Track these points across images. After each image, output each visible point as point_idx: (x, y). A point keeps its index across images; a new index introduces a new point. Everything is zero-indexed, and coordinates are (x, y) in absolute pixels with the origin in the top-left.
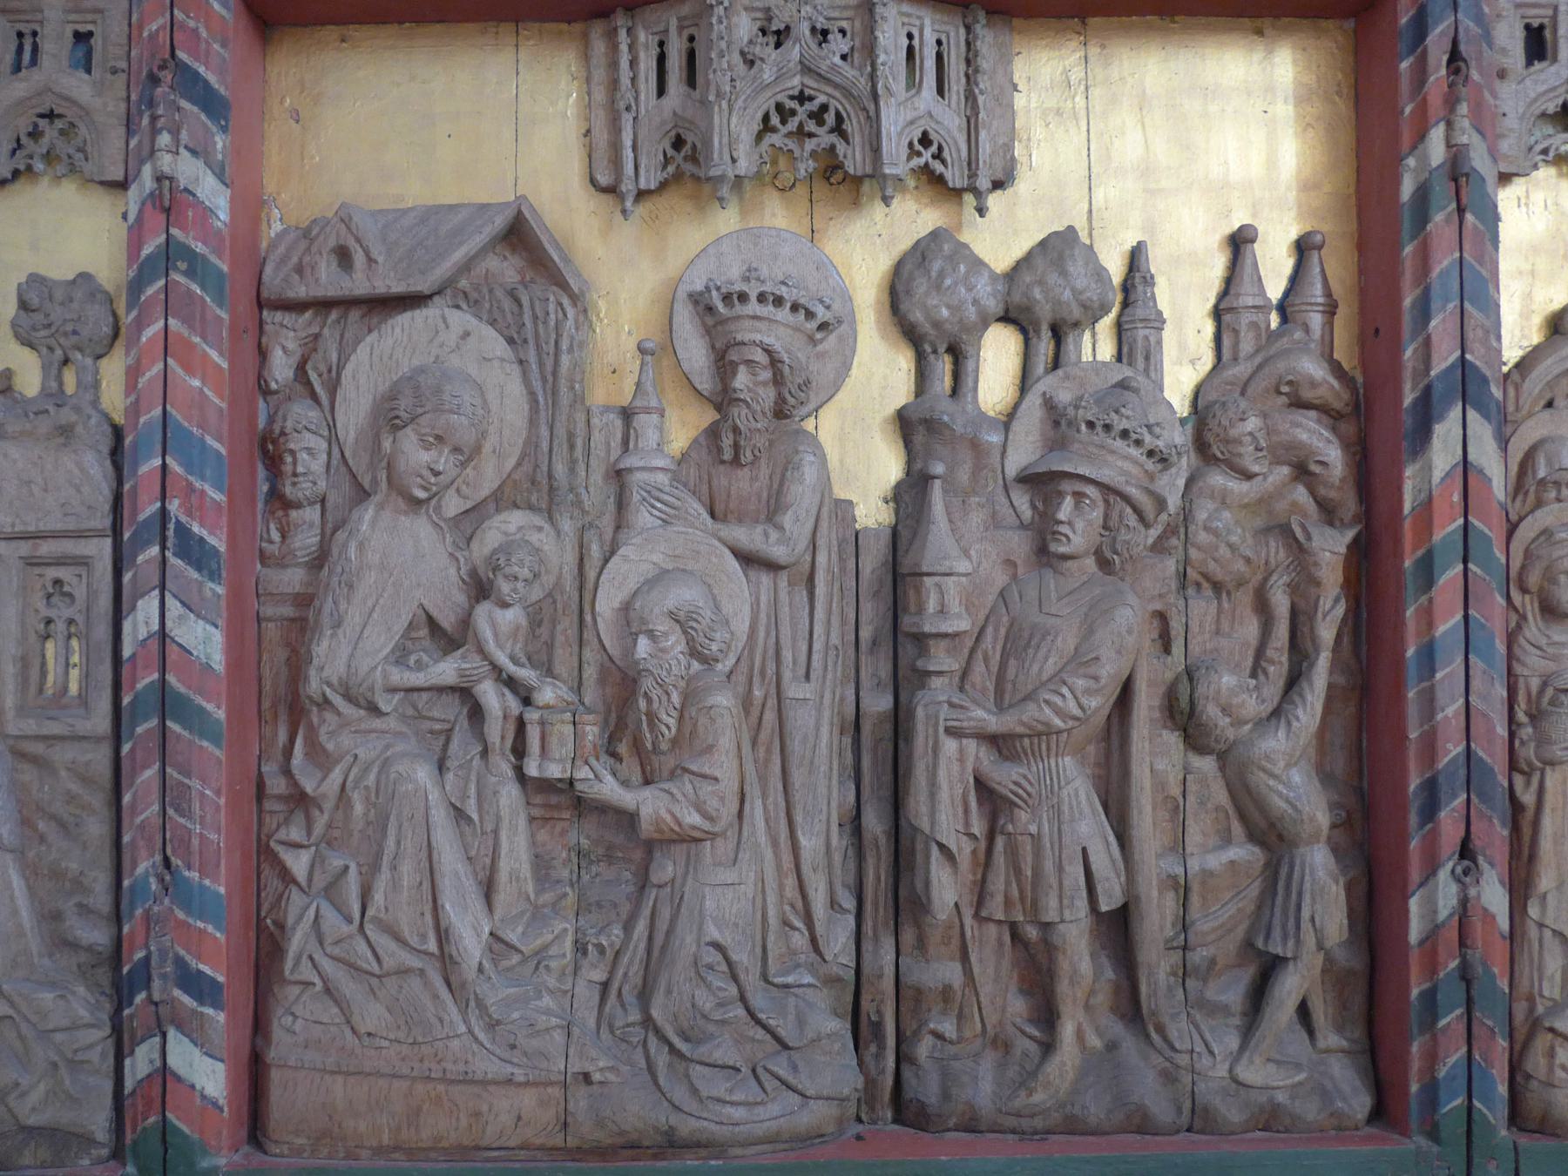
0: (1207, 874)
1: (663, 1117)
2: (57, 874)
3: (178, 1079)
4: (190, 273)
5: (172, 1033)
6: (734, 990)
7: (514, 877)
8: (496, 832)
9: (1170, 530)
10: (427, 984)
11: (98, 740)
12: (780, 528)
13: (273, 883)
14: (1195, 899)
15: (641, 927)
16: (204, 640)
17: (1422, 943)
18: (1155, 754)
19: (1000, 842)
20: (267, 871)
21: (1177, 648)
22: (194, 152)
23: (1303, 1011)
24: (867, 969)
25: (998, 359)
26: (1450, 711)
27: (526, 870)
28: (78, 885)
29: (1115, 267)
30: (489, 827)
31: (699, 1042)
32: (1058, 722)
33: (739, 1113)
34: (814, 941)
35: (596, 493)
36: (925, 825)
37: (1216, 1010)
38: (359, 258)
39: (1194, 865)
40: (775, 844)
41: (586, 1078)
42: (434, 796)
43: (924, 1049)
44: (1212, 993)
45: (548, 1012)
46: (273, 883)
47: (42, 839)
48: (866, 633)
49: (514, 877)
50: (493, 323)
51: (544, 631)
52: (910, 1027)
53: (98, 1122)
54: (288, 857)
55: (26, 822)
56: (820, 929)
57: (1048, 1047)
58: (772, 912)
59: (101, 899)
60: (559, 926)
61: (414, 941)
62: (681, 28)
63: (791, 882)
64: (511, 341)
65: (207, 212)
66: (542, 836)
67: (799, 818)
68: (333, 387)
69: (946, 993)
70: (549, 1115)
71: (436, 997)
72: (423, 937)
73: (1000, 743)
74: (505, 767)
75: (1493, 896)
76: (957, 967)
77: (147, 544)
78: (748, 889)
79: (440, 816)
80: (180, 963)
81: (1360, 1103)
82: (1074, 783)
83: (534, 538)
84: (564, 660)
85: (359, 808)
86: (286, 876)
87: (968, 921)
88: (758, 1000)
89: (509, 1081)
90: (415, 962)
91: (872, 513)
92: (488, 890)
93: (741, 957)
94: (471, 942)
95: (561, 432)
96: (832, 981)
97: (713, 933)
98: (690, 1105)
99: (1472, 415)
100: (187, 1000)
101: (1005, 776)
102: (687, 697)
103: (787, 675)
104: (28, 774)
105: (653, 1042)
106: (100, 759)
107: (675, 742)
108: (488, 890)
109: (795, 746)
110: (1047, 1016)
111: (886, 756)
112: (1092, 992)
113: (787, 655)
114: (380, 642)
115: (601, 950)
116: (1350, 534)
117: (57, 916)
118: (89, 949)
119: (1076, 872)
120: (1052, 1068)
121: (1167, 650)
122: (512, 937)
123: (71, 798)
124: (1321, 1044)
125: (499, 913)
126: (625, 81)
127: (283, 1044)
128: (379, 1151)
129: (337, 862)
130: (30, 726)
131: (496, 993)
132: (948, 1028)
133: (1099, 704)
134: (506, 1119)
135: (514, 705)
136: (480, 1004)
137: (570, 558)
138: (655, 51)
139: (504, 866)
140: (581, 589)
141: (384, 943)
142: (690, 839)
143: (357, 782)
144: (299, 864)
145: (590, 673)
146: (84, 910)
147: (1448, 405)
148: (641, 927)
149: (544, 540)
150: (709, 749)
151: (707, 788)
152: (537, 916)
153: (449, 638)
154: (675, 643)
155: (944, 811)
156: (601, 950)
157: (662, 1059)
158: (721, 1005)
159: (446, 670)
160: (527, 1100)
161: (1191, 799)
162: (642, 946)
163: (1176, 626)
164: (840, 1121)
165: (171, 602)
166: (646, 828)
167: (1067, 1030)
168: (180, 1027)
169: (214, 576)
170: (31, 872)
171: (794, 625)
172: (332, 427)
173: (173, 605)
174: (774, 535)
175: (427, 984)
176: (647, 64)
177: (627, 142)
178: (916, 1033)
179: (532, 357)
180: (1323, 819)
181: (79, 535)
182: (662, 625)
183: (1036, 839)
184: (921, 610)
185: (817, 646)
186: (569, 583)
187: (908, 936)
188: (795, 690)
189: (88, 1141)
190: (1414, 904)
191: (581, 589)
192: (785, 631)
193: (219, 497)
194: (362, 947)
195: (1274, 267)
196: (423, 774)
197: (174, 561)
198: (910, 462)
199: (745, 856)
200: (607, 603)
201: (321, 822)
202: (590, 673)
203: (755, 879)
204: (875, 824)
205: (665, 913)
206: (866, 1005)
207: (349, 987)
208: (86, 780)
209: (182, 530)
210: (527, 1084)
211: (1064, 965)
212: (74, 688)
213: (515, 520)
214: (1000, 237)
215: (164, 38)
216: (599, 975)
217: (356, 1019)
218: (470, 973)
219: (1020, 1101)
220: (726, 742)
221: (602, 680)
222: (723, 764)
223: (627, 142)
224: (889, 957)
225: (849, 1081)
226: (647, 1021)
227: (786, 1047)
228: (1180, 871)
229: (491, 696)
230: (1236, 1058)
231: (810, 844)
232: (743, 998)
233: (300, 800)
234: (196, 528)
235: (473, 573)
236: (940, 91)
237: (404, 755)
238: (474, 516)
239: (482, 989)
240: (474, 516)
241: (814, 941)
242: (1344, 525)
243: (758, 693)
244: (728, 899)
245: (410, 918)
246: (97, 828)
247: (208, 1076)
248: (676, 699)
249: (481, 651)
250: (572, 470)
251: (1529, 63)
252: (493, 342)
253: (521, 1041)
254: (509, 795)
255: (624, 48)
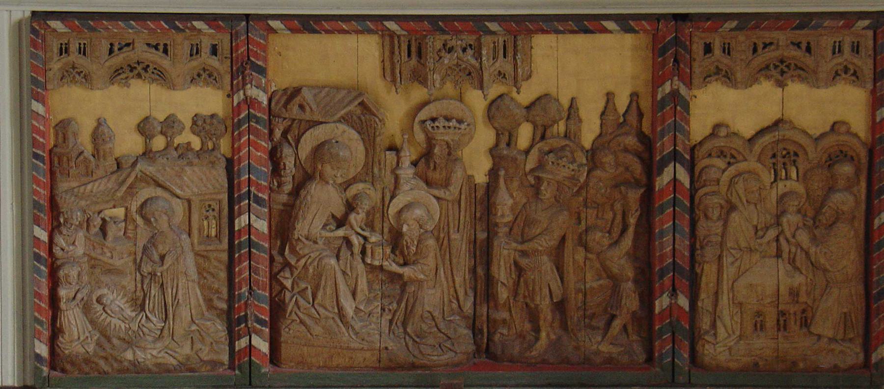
0: (592, 288)
1: (411, 359)
2: (210, 288)
3: (255, 348)
4: (257, 122)
5: (253, 336)
6: (434, 323)
7: (362, 291)
8: (357, 278)
9: (581, 188)
10: (335, 321)
11: (224, 251)
12: (449, 190)
13: (278, 288)
14: (588, 296)
15: (403, 305)
16: (262, 226)
17: (659, 313)
18: (575, 256)
19: (522, 279)
20: (274, 283)
21: (583, 223)
22: (257, 87)
23: (625, 327)
24: (478, 314)
25: (525, 134)
26: (668, 249)
27: (366, 288)
28: (218, 291)
29: (566, 103)
30: (354, 276)
31: (423, 338)
32: (540, 248)
33: (435, 358)
34: (459, 306)
35: (389, 179)
36: (497, 276)
37: (594, 328)
38: (308, 108)
39: (588, 286)
40: (447, 278)
41: (386, 348)
42: (337, 268)
43: (497, 337)
44: (594, 323)
45: (374, 329)
46: (277, 288)
47: (205, 278)
48: (478, 215)
49: (362, 291)
50: (353, 127)
51: (371, 217)
52: (492, 330)
53: (225, 358)
54: (285, 282)
55: (199, 273)
56: (462, 303)
57: (537, 339)
58: (446, 300)
59: (225, 295)
60: (376, 304)
61: (330, 309)
62: (416, 40)
63: (452, 290)
64: (359, 133)
65: (260, 103)
66: (370, 276)
67: (455, 273)
68: (298, 142)
69: (504, 321)
70: (375, 358)
71: (338, 325)
72: (333, 308)
73: (524, 254)
74: (358, 258)
75: (683, 302)
76: (508, 313)
77: (244, 200)
78: (439, 294)
79: (339, 275)
80: (256, 316)
81: (642, 357)
82: (547, 264)
83: (368, 192)
84: (378, 226)
85: (311, 271)
86: (284, 287)
87: (511, 301)
88: (442, 326)
89: (362, 349)
90: (331, 315)
91: (481, 178)
92: (354, 294)
93: (436, 314)
94: (349, 310)
95: (376, 160)
96: (465, 317)
97: (428, 309)
98: (419, 356)
99: (677, 165)
100: (258, 326)
101: (524, 262)
102: (419, 242)
103: (452, 231)
104: (201, 261)
105: (407, 337)
106: (225, 256)
107: (415, 254)
108: (354, 294)
109: (454, 251)
110: (537, 330)
111: (483, 253)
112: (553, 322)
113: (452, 225)
114: (318, 223)
115: (390, 310)
116: (642, 190)
117: (211, 300)
118: (221, 310)
119: (546, 291)
120: (538, 345)
121: (580, 223)
122: (362, 308)
123: (216, 267)
124: (631, 339)
125: (357, 300)
126: (397, 53)
127: (285, 335)
128: (319, 367)
129: (303, 286)
130: (203, 247)
131: (358, 325)
132: (505, 332)
133: (554, 243)
134: (361, 359)
135: (362, 241)
136: (353, 329)
137: (380, 196)
138: (407, 44)
139: (359, 288)
140: (383, 205)
141: (322, 311)
142: (420, 282)
143: (310, 264)
144: (288, 283)
145: (386, 230)
146: (219, 298)
147: (670, 163)
148: (403, 305)
149: (371, 192)
150: (427, 257)
151: (425, 268)
152: (369, 301)
153: (341, 222)
154: (415, 226)
155: (502, 273)
156: (390, 310)
157: (410, 343)
158: (430, 328)
159: (341, 232)
160: (368, 355)
161: (588, 266)
162: (403, 312)
163: (583, 215)
164: (467, 359)
165: (252, 215)
166: (406, 278)
167: (543, 334)
168: (256, 333)
169: (264, 206)
170: (202, 287)
171: (454, 216)
172: (297, 154)
173: (253, 217)
174: (447, 193)
175: (335, 321)
176: (404, 47)
177: (398, 71)
178: (494, 333)
179: (367, 139)
180: (630, 274)
181: (219, 193)
182: (411, 222)
183: (534, 280)
184: (496, 215)
185: (461, 222)
186: (379, 205)
187: (492, 304)
188: (454, 236)
189: (222, 364)
190: (657, 303)
191: (383, 205)
192: (451, 219)
193: (265, 184)
194: (313, 311)
195: (622, 103)
196: (333, 261)
197: (253, 205)
198: (494, 164)
199: (437, 286)
200: (392, 211)
201: (296, 273)
202: (386, 230)
203: (440, 288)
204: (480, 271)
205: (411, 300)
206: (477, 323)
207: (308, 321)
208: (220, 262)
209: (256, 196)
210: (368, 350)
211: (542, 316)
212: (213, 233)
213: (361, 186)
214: (526, 95)
215: (245, 53)
216: (389, 317)
217: (312, 331)
218: (350, 320)
219: (527, 354)
220: (432, 254)
221: (390, 232)
222: (431, 262)
223: (398, 71)
224: (485, 309)
225: (472, 348)
226: (405, 332)
227: (449, 338)
228: (583, 287)
229: (356, 241)
230: (599, 343)
231: (458, 280)
232: (436, 325)
233: (287, 264)
234: (260, 195)
235: (347, 201)
236: (505, 57)
237: (327, 256)
238: (347, 185)
239: (353, 323)
240: (347, 185)
241: (459, 306)
242: (641, 187)
243: (442, 235)
244: (431, 298)
245: (329, 302)
246: (223, 275)
247: (262, 345)
248: (416, 243)
249: (352, 228)
250: (380, 169)
251: (705, 54)
252: (354, 135)
253: (366, 338)
254: (361, 267)
255: (396, 42)
